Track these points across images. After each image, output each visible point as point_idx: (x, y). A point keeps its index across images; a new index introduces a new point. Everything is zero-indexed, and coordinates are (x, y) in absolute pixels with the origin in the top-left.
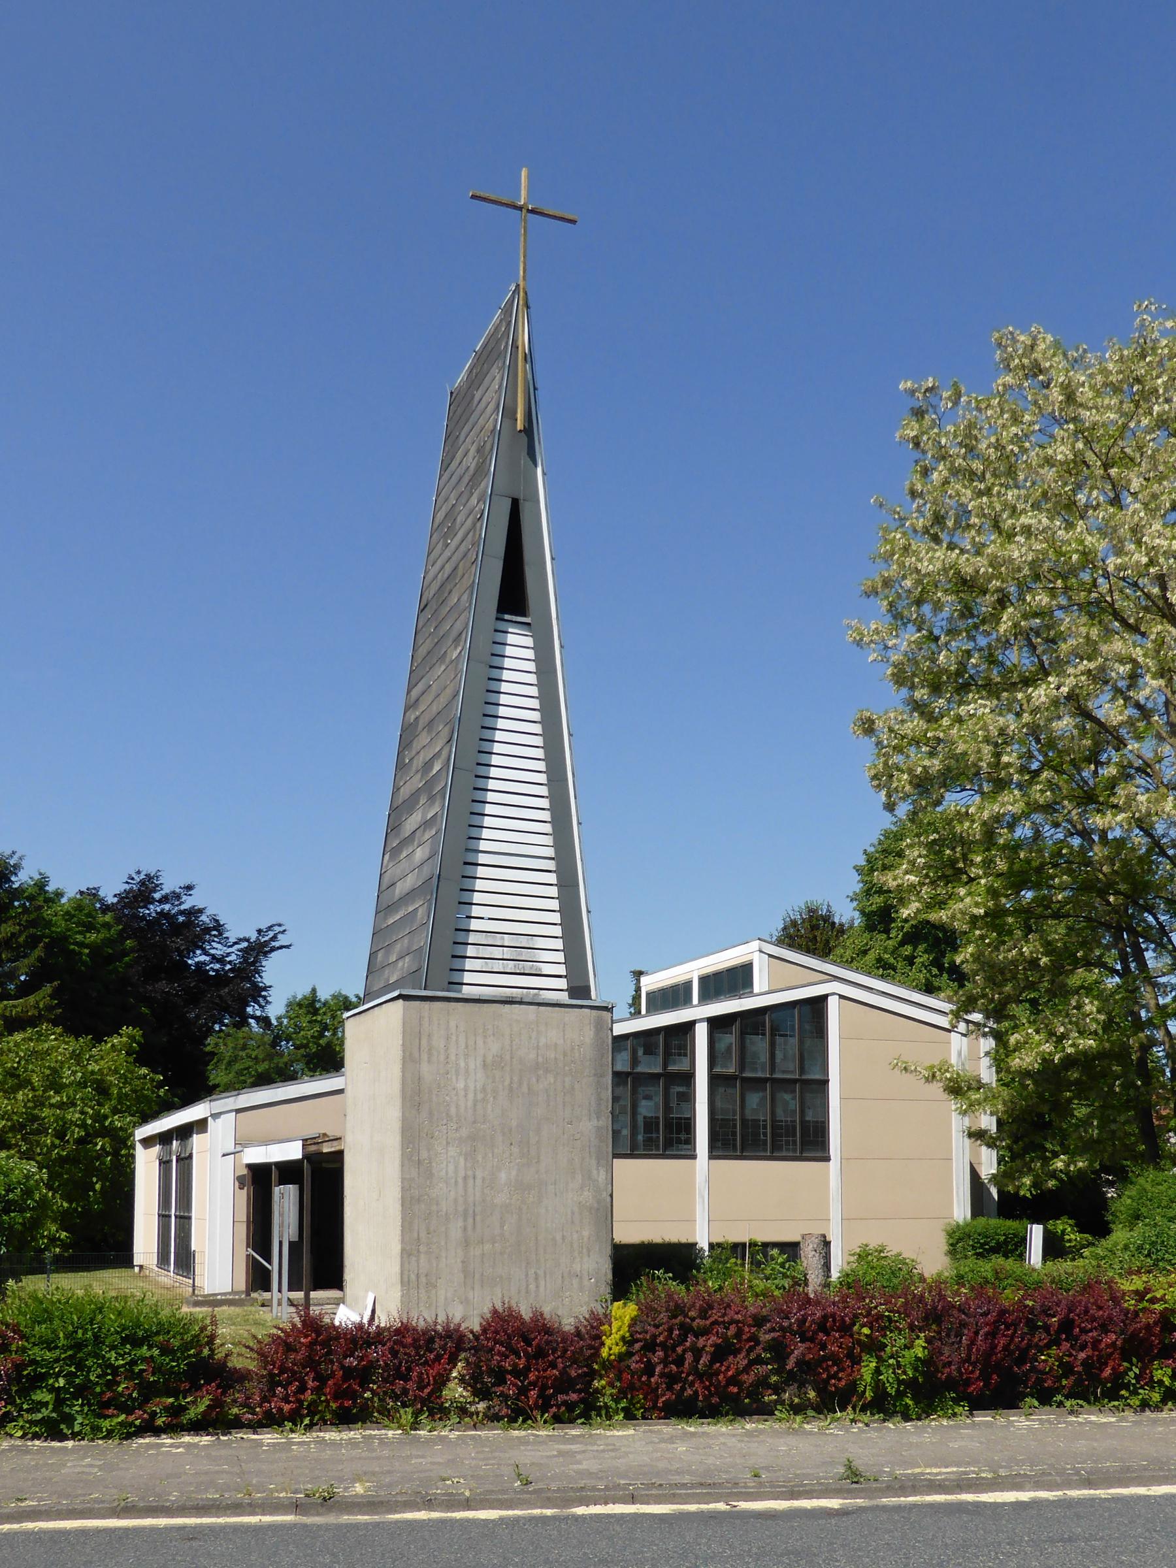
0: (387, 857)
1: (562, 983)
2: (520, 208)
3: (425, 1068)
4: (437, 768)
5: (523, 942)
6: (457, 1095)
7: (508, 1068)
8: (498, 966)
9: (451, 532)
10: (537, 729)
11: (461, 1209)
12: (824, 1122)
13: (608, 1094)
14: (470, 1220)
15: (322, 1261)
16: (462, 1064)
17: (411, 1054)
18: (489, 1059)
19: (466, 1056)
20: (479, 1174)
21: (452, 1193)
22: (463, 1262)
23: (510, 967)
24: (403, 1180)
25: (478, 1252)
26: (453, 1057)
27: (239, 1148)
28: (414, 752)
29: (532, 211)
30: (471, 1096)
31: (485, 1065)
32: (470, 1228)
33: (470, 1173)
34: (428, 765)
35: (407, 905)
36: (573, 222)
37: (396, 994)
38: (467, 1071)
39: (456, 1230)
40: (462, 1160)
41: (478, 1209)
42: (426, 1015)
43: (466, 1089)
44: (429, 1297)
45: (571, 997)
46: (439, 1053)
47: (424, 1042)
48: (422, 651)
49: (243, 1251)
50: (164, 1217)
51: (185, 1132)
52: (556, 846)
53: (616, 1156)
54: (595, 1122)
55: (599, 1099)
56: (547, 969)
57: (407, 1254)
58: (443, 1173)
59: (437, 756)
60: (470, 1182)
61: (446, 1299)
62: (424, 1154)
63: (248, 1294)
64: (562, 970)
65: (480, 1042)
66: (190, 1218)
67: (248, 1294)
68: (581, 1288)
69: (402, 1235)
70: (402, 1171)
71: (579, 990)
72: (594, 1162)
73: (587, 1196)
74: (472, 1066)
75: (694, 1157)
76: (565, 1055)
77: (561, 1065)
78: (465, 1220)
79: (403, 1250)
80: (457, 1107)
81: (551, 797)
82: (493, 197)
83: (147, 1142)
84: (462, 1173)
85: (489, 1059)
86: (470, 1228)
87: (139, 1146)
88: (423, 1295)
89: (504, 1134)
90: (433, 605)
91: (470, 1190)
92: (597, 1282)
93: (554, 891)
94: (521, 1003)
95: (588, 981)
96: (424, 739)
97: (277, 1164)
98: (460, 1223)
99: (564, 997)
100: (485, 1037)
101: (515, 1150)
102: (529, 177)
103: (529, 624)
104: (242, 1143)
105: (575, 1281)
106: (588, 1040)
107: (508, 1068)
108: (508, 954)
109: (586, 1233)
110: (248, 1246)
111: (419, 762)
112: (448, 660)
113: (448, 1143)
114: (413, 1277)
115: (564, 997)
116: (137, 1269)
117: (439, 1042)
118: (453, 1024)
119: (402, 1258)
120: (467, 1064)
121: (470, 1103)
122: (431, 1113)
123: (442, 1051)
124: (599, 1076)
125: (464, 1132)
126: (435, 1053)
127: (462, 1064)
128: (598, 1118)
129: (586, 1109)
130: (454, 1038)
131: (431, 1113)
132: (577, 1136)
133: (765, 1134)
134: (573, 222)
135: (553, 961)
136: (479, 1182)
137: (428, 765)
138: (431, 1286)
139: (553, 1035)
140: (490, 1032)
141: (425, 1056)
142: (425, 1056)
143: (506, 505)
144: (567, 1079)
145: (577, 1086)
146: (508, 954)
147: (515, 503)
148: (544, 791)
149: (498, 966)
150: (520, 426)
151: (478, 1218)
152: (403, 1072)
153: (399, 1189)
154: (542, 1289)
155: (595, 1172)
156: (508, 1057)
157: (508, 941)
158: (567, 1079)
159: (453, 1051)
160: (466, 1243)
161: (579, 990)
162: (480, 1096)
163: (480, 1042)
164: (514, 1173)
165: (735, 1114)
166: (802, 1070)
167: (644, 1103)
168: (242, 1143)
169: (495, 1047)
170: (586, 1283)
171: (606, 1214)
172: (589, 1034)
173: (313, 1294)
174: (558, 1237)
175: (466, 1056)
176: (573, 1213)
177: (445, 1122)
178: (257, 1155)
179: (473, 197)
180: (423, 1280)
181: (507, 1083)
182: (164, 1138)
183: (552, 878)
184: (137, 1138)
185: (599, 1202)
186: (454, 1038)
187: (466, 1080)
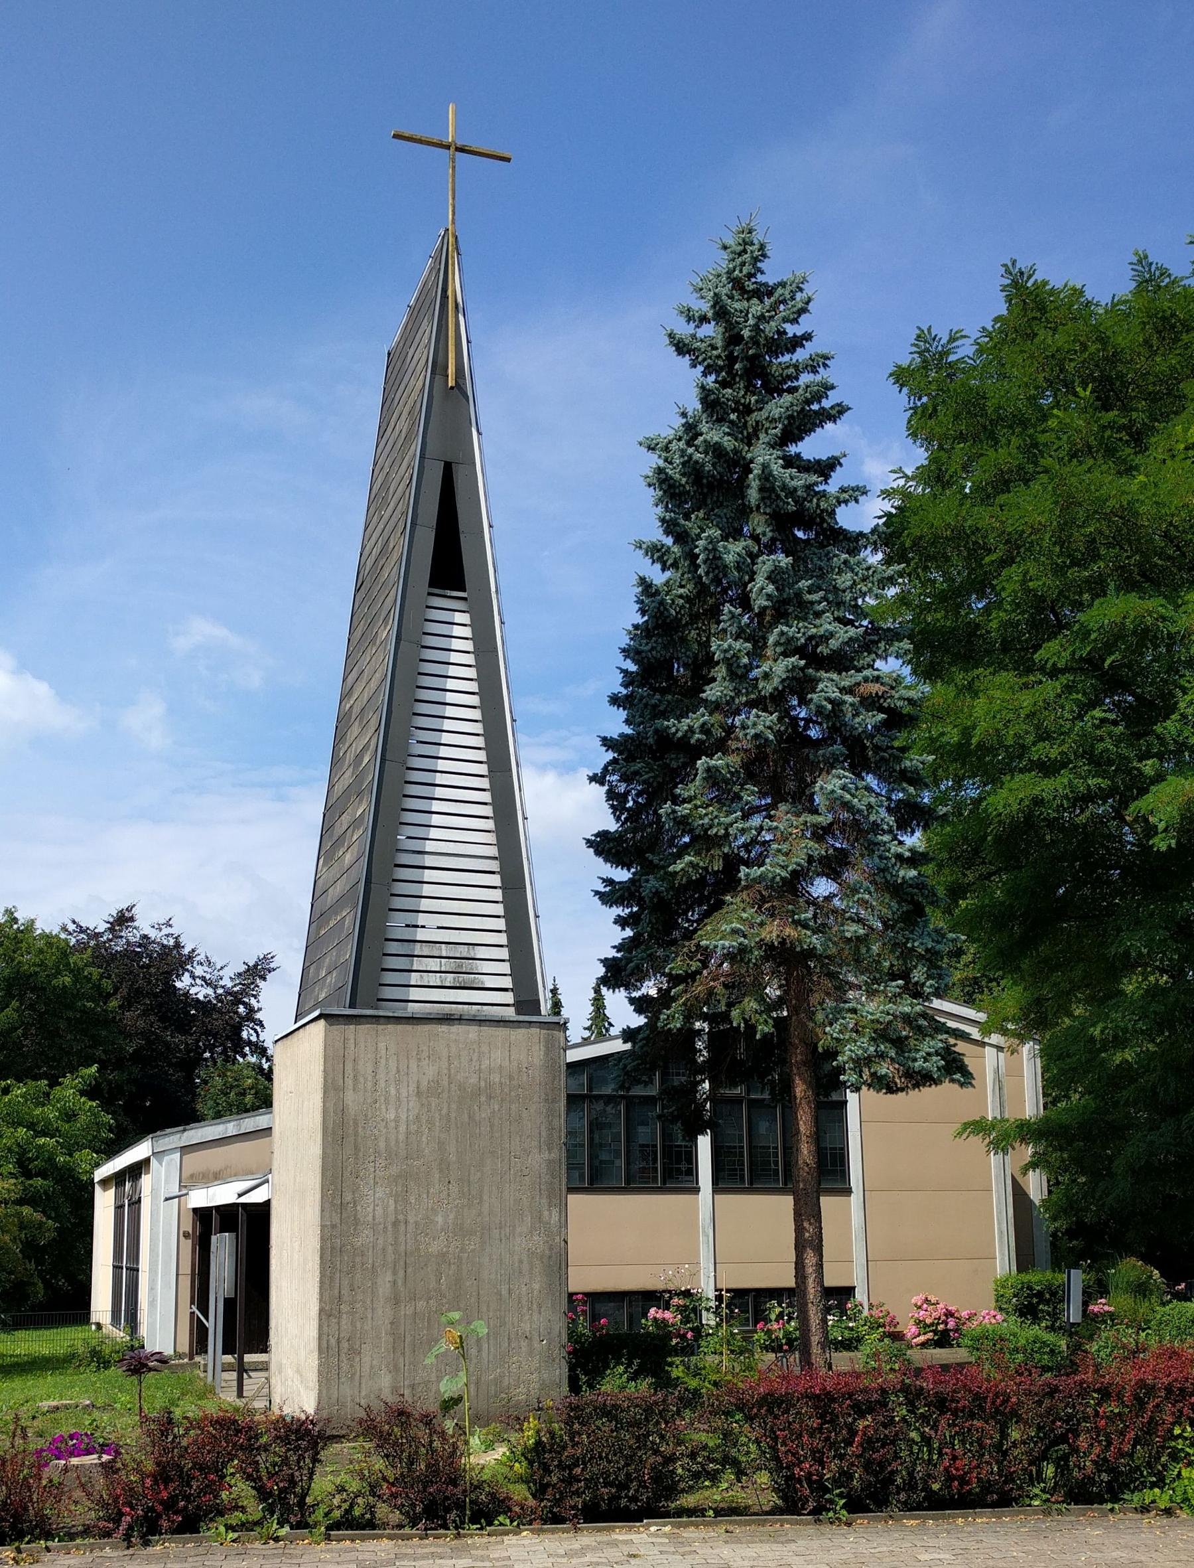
0: (321, 861)
1: (509, 998)
2: (448, 147)
3: (350, 1097)
4: (366, 760)
5: (463, 951)
6: (386, 1127)
7: (445, 1095)
8: (434, 979)
9: (385, 502)
10: (476, 714)
11: (390, 1258)
12: (843, 1149)
13: (560, 1122)
14: (401, 1273)
15: (246, 1323)
16: (393, 1092)
17: (334, 1079)
18: (424, 1084)
19: (398, 1082)
20: (411, 1219)
21: (380, 1241)
22: (392, 1323)
23: (449, 979)
24: (323, 1227)
25: (410, 1311)
26: (382, 1084)
27: (184, 1192)
28: (347, 745)
29: (457, 149)
30: (403, 1128)
31: (419, 1094)
32: (400, 1282)
33: (401, 1217)
34: (359, 757)
35: (336, 914)
36: (508, 160)
37: (316, 1013)
38: (399, 1099)
39: (385, 1281)
40: (391, 1202)
41: (410, 1260)
42: (352, 1037)
43: (397, 1120)
44: (352, 1366)
45: (518, 1013)
46: (366, 1079)
47: (349, 1066)
48: (358, 634)
49: (186, 1308)
50: (117, 1268)
51: (136, 1171)
52: (499, 844)
53: (571, 1190)
54: (546, 1155)
55: (551, 1129)
56: (489, 982)
57: (325, 1314)
58: (370, 1218)
59: (365, 748)
60: (402, 1228)
61: (372, 1367)
62: (348, 1197)
63: (191, 1358)
64: (507, 982)
65: (413, 1065)
66: (138, 1270)
67: (191, 1358)
68: (531, 1353)
69: (321, 1294)
70: (322, 1217)
71: (527, 1003)
72: (544, 1201)
73: (538, 1242)
74: (405, 1094)
75: (696, 1190)
76: (511, 1078)
77: (506, 1090)
78: (395, 1273)
79: (321, 1310)
80: (387, 1140)
81: (493, 790)
82: (418, 134)
83: (105, 1183)
84: (391, 1218)
85: (424, 1084)
86: (400, 1282)
87: (98, 1189)
88: (345, 1366)
89: (441, 1171)
90: (367, 585)
91: (402, 1239)
92: (549, 1344)
93: (497, 895)
94: (447, 1019)
95: (537, 994)
96: (355, 729)
97: (217, 1208)
98: (389, 1277)
99: (510, 1013)
100: (419, 1059)
101: (454, 1188)
102: (456, 114)
103: (464, 599)
104: (188, 1182)
105: (524, 1343)
106: (537, 1061)
107: (445, 1095)
108: (446, 965)
109: (536, 1286)
110: (192, 1303)
111: (350, 756)
112: (378, 643)
113: (376, 1183)
114: (333, 1341)
115: (510, 1013)
116: (94, 1327)
117: (366, 1068)
118: (382, 1046)
119: (320, 1320)
120: (398, 1091)
121: (401, 1137)
122: (356, 1148)
123: (370, 1078)
124: (550, 1101)
125: (394, 1170)
126: (362, 1080)
127: (393, 1092)
128: (550, 1150)
129: (535, 1138)
130: (383, 1061)
131: (356, 1148)
132: (526, 1172)
133: (776, 1163)
134: (508, 160)
135: (496, 971)
136: (411, 1228)
137: (359, 757)
138: (354, 1352)
139: (498, 1057)
140: (425, 1054)
141: (349, 1082)
142: (349, 1082)
143: (435, 474)
144: (513, 1107)
145: (525, 1114)
146: (446, 965)
147: (448, 468)
148: (485, 783)
149: (434, 979)
150: (451, 383)
151: (409, 1270)
152: (324, 1102)
153: (318, 1238)
154: (484, 1354)
155: (546, 1213)
156: (445, 1083)
157: (444, 951)
158: (513, 1107)
159: (382, 1076)
160: (396, 1301)
161: (527, 1003)
162: (413, 1128)
163: (413, 1065)
164: (452, 1216)
165: (741, 1141)
166: (590, 1089)
167: (641, 1129)
168: (188, 1182)
169: (431, 1071)
170: (536, 1345)
171: (559, 1262)
172: (538, 1055)
173: (248, 1358)
174: (504, 1292)
175: (398, 1082)
176: (521, 1262)
177: (372, 1158)
178: (201, 1198)
179: (395, 136)
180: (345, 1345)
181: (444, 1112)
182: (118, 1179)
183: (496, 880)
184: (96, 1180)
185: (551, 1249)
186: (383, 1061)
187: (397, 1110)
